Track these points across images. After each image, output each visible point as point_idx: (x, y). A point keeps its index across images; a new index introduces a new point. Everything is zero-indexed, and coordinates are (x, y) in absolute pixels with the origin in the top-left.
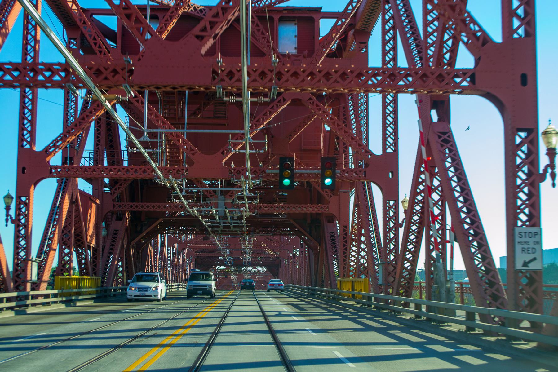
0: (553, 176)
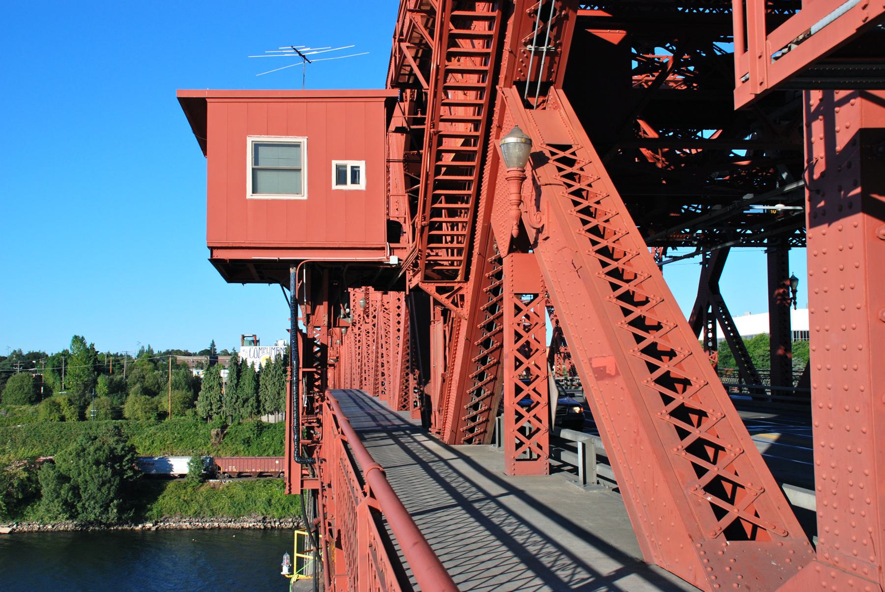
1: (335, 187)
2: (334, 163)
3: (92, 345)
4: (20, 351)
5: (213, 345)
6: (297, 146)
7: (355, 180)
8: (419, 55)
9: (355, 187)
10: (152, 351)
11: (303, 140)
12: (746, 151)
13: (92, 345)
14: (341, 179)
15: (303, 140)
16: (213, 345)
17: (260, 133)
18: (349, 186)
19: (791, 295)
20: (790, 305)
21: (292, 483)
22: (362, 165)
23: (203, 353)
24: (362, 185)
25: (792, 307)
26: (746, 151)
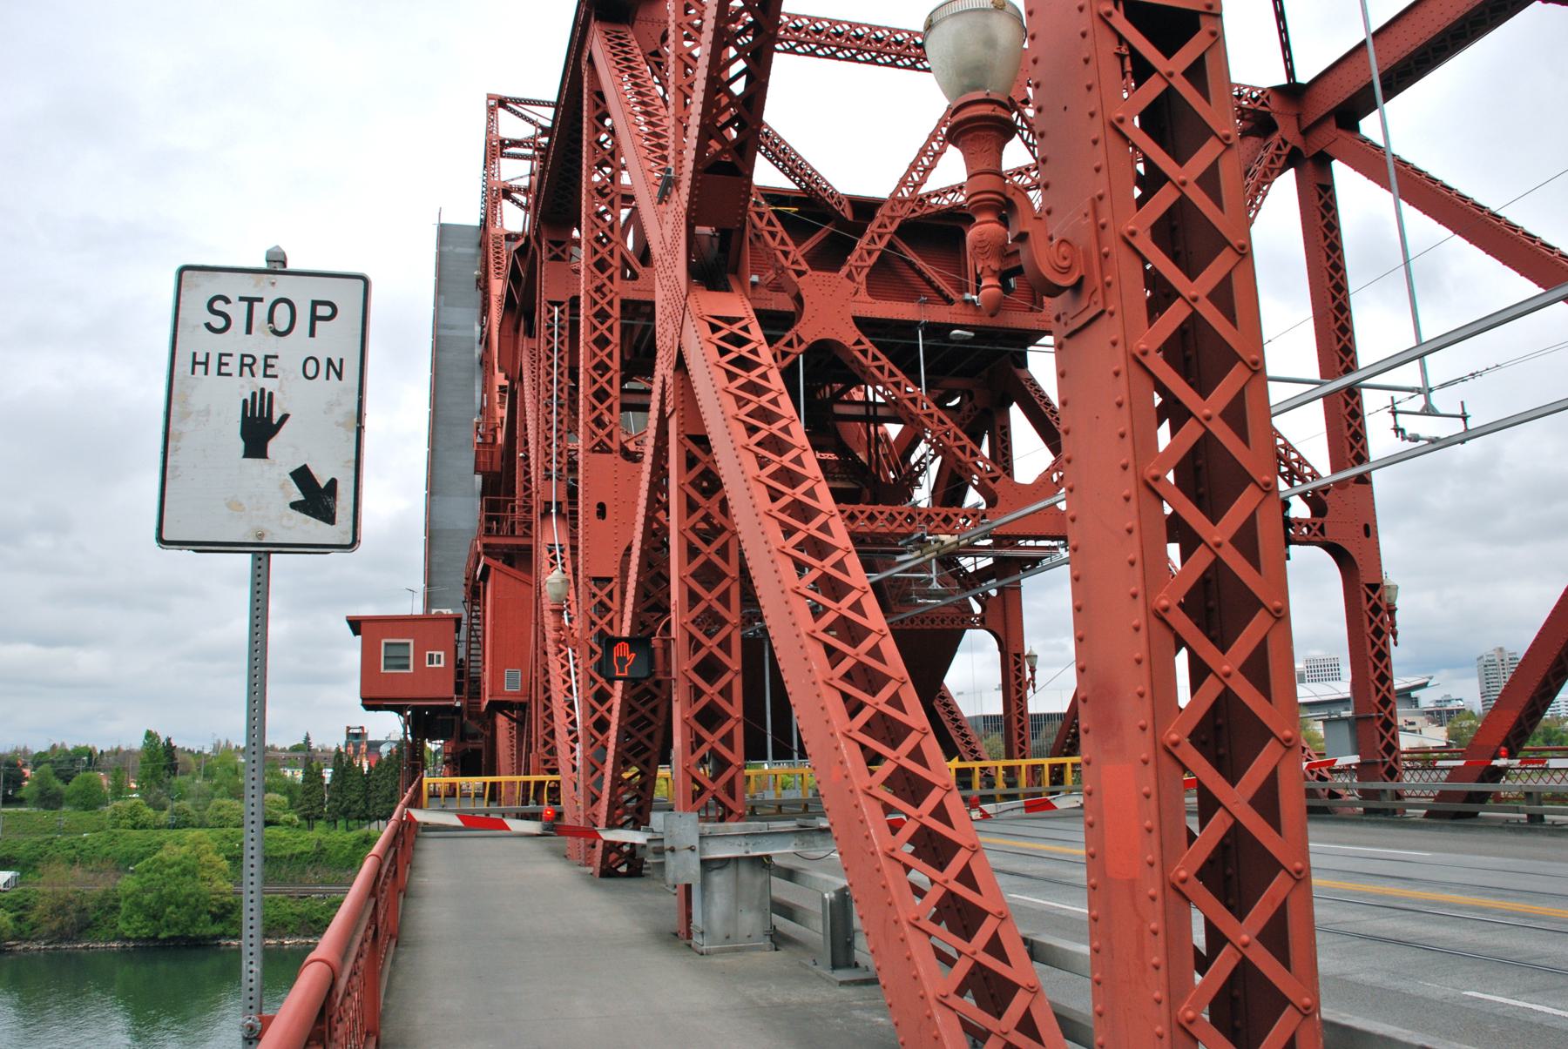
0: (1034, 686)
1: (428, 666)
2: (428, 653)
3: (169, 740)
4: (63, 744)
5: (307, 738)
6: (408, 644)
7: (439, 662)
8: (492, 816)
9: (438, 666)
10: (231, 746)
11: (411, 642)
12: (1015, 404)
13: (169, 740)
14: (431, 662)
15: (411, 642)
16: (307, 738)
17: (388, 638)
18: (435, 665)
19: (1028, 675)
20: (1028, 688)
21: (901, 70)
22: (442, 654)
23: (295, 749)
24: (442, 665)
25: (1030, 692)
26: (1015, 404)
